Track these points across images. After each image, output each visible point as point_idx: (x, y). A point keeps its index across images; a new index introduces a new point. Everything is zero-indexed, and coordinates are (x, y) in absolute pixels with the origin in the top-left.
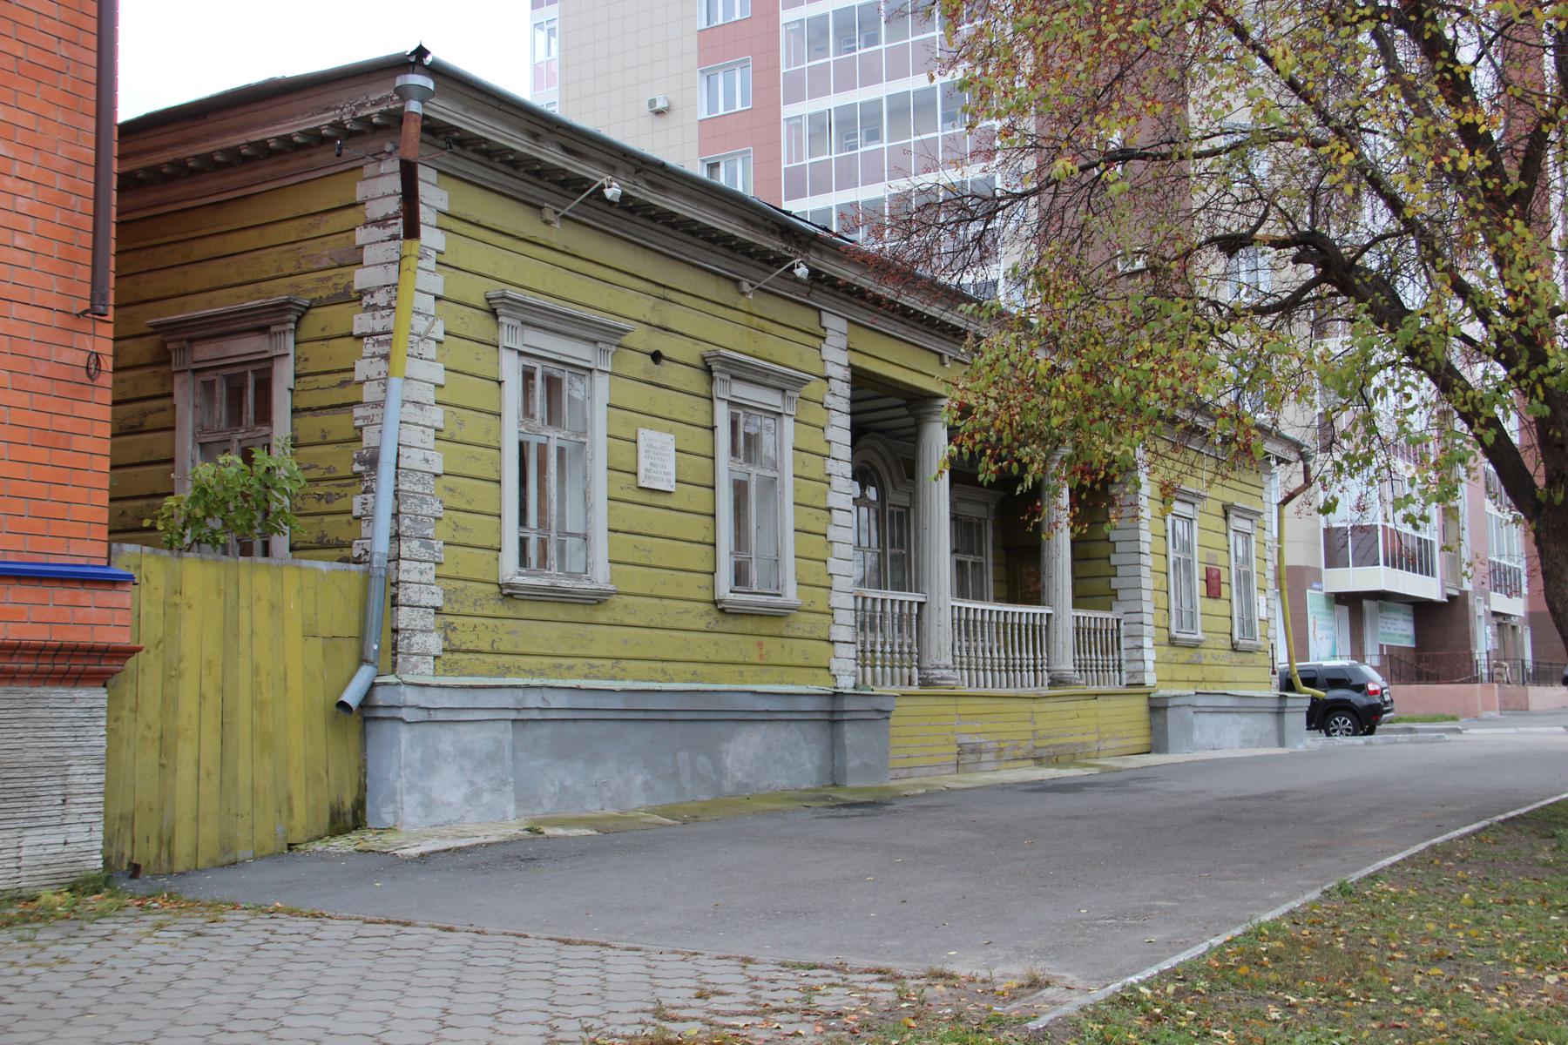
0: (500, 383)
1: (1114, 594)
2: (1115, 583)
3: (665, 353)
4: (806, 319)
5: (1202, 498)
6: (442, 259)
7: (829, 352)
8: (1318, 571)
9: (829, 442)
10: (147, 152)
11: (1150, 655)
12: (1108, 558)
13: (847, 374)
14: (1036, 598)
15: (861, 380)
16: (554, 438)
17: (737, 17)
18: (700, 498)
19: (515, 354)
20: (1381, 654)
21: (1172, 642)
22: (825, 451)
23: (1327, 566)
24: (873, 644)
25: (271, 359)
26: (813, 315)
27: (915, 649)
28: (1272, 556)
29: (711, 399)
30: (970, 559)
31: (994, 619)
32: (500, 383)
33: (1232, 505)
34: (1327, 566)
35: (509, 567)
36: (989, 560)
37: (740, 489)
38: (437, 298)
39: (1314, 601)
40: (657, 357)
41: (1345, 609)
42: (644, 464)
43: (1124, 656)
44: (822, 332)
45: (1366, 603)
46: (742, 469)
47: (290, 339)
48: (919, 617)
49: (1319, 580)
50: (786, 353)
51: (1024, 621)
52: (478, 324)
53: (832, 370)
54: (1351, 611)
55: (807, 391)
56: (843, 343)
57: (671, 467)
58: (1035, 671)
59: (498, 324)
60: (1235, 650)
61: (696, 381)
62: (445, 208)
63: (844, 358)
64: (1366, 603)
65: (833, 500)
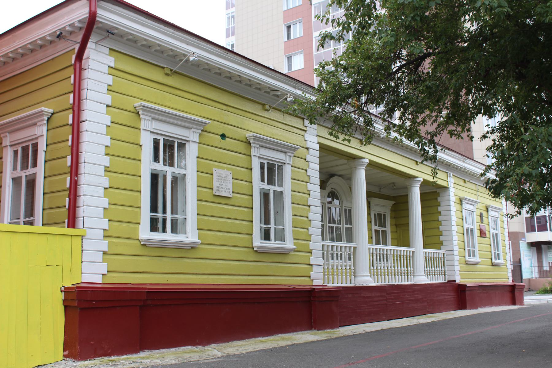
0: (141, 146)
1: (442, 243)
2: (442, 238)
3: (227, 135)
4: (297, 123)
5: (477, 202)
6: (110, 88)
7: (308, 137)
8: (524, 234)
9: (309, 176)
10: (375, 220)
11: (457, 268)
12: (439, 228)
13: (317, 147)
14: (407, 244)
15: (323, 148)
16: (169, 171)
17: (298, 36)
18: (242, 199)
19: (149, 132)
20: (549, 266)
21: (467, 263)
22: (307, 180)
23: (527, 232)
24: (341, 266)
25: (37, 138)
26: (300, 121)
27: (353, 268)
28: (506, 230)
29: (251, 156)
30: (381, 229)
31: (396, 253)
32: (141, 146)
33: (489, 206)
34: (527, 232)
35: (258, 242)
36: (388, 229)
37: (265, 196)
38: (108, 106)
39: (523, 246)
40: (223, 136)
41: (535, 248)
42: (216, 184)
43: (446, 269)
44: (304, 128)
45: (543, 246)
46: (265, 186)
47: (45, 128)
48: (413, 256)
49: (524, 237)
50: (291, 138)
51: (402, 254)
52: (125, 117)
53: (309, 145)
54: (537, 249)
55: (297, 153)
56: (315, 132)
57: (230, 186)
58: (408, 275)
59: (140, 119)
60: (493, 265)
61: (241, 147)
62: (112, 65)
63: (316, 139)
64: (543, 246)
65: (311, 201)
